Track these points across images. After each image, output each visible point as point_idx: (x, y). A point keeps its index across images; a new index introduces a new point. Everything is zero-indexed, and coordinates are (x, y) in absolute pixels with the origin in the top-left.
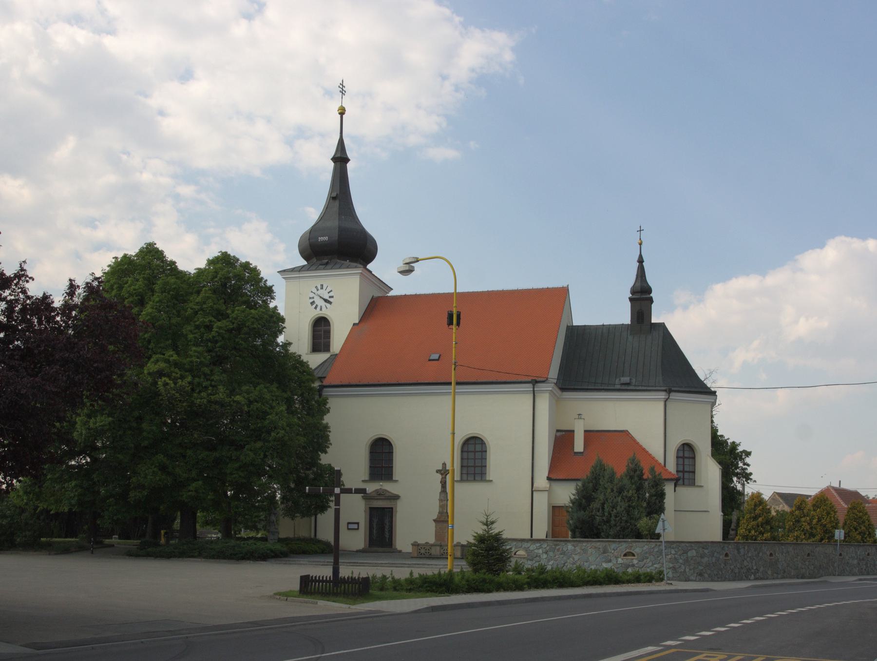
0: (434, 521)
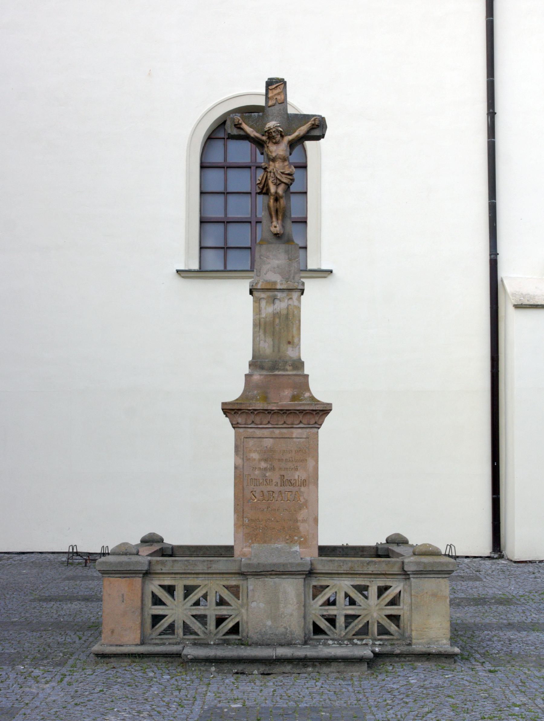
0: (229, 410)
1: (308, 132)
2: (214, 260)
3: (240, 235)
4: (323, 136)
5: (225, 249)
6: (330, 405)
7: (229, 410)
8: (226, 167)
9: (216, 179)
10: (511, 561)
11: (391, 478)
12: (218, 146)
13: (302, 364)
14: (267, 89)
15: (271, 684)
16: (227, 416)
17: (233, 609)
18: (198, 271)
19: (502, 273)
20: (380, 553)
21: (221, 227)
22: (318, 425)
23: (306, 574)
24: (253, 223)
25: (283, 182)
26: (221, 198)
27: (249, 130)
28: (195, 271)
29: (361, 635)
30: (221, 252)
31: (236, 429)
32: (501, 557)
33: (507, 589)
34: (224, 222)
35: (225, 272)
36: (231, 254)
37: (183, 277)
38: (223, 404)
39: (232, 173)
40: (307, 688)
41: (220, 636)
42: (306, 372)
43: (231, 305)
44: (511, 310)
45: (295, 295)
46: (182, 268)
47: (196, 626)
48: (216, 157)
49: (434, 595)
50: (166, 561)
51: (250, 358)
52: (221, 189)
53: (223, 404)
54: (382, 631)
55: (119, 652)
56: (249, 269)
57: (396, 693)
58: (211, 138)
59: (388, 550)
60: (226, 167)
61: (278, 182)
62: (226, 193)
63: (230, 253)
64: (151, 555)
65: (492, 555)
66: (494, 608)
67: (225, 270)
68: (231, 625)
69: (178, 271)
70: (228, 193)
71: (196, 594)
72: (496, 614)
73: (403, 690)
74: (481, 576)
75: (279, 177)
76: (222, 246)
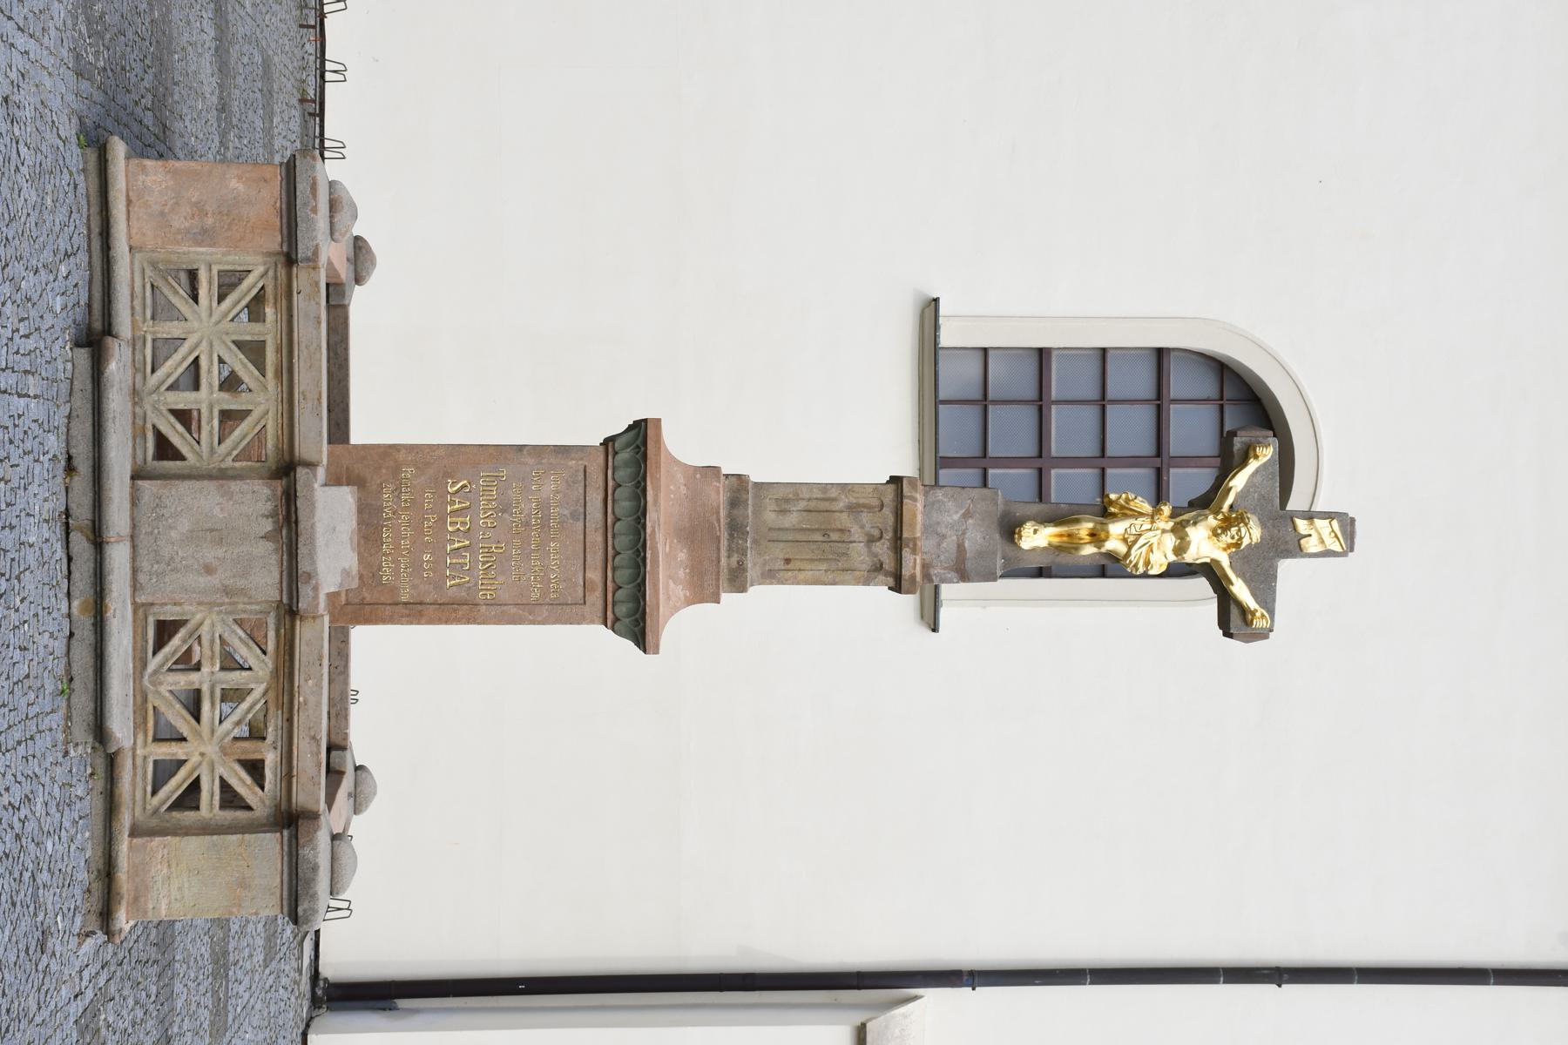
0: (641, 434)
1: (1239, 604)
2: (959, 378)
3: (1011, 431)
4: (1228, 634)
5: (984, 402)
6: (656, 652)
7: (641, 434)
8: (1159, 401)
9: (1133, 382)
10: (308, 1026)
11: (491, 776)
12: (1206, 386)
13: (742, 589)
14: (1329, 516)
15: (46, 535)
16: (630, 428)
17: (212, 448)
18: (936, 343)
19: (932, 997)
20: (334, 753)
21: (1030, 392)
22: (614, 625)
23: (290, 606)
24: (1038, 463)
25: (1130, 548)
26: (1094, 394)
27: (1239, 482)
28: (936, 337)
29: (166, 783)
30: (978, 395)
31: (602, 449)
32: (316, 1002)
33: (246, 1023)
34: (1041, 399)
35: (932, 399)
36: (972, 414)
37: (923, 312)
38: (659, 420)
39: (1146, 414)
40: (36, 615)
41: (153, 418)
42: (724, 596)
43: (865, 436)
44: (858, 1018)
45: (891, 581)
46: (942, 311)
47: (174, 366)
48: (1181, 382)
49: (243, 884)
50: (318, 304)
51: (755, 477)
52: (1110, 394)
53: (659, 420)
54: (164, 771)
55: (112, 194)
56: (941, 454)
57: (24, 812)
58: (1224, 371)
59: (341, 773)
60: (1159, 401)
61: (1132, 539)
62: (1102, 402)
63: (975, 411)
64: (330, 263)
65: (321, 983)
66: (208, 1000)
67: (938, 402)
68: (175, 440)
69: (936, 300)
70: (1103, 408)
71: (245, 366)
72: (193, 1007)
73: (31, 825)
74: (274, 964)
75: (1141, 541)
76: (991, 396)
